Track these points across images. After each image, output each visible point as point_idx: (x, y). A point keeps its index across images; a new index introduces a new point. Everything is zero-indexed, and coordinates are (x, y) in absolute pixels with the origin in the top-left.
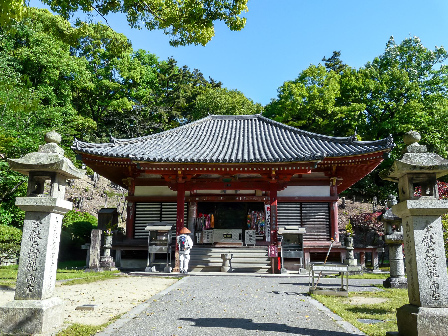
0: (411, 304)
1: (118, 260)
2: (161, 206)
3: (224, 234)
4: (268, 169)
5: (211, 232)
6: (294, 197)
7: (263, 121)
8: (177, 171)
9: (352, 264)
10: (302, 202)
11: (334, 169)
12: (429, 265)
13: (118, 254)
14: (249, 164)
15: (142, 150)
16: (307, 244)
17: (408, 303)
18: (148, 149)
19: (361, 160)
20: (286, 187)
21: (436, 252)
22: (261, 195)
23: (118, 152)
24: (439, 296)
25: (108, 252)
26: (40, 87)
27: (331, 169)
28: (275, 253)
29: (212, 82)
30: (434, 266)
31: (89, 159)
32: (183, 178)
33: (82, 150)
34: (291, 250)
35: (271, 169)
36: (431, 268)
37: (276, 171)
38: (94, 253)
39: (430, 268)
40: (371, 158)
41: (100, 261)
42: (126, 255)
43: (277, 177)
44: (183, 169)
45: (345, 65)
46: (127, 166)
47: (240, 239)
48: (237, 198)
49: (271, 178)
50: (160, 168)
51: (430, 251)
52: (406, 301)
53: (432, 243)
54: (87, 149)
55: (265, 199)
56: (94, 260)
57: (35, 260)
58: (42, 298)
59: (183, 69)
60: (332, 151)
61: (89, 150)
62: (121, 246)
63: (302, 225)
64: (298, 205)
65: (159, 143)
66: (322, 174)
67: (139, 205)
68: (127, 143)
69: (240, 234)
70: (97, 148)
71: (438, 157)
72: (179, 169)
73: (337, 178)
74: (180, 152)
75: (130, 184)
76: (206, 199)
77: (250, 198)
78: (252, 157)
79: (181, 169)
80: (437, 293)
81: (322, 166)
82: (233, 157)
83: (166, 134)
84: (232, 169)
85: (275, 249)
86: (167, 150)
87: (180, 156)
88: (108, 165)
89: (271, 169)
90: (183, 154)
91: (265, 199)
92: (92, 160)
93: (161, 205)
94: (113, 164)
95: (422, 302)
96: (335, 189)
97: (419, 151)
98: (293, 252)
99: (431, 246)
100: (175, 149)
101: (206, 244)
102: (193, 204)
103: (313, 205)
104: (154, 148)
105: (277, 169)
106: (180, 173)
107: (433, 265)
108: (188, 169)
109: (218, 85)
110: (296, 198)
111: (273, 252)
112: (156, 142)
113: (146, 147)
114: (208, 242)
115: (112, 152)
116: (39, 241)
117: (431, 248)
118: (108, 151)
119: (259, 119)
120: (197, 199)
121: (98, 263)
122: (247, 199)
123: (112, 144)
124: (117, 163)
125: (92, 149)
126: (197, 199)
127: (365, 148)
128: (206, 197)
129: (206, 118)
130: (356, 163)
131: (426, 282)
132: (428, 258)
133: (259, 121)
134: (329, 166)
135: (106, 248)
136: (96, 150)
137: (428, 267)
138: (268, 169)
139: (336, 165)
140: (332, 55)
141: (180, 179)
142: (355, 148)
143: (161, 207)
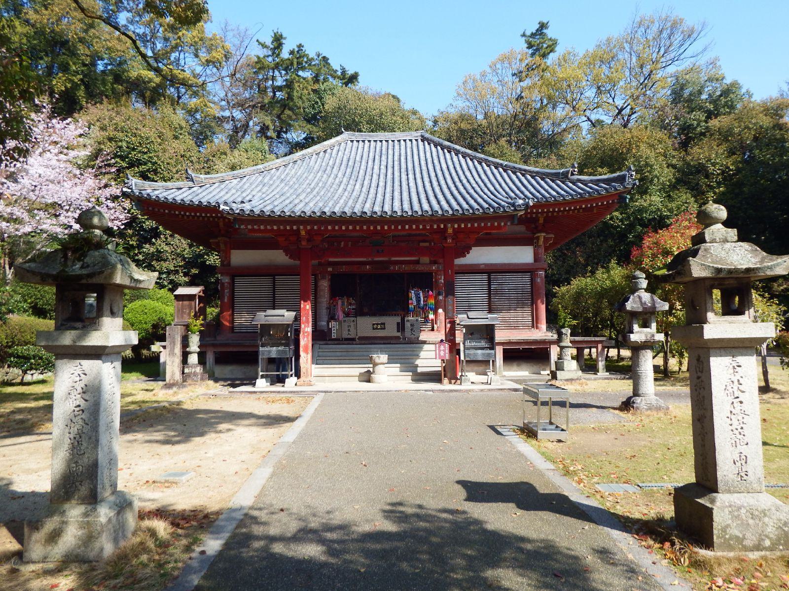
0: (698, 484)
1: (210, 367)
3: (374, 324)
4: (442, 226)
5: (353, 321)
7: (430, 142)
8: (298, 229)
9: (569, 369)
10: (491, 271)
11: (541, 221)
12: (733, 427)
13: (210, 358)
14: (423, 232)
15: (239, 193)
16: (501, 336)
17: (692, 479)
18: (249, 191)
19: (584, 206)
20: (468, 253)
21: (744, 407)
23: (201, 196)
24: (746, 475)
25: (193, 359)
27: (536, 220)
29: (344, 72)
30: (742, 428)
31: (153, 209)
32: (309, 240)
36: (736, 432)
37: (454, 229)
38: (173, 362)
39: (736, 432)
40: (600, 204)
41: (183, 373)
42: (223, 359)
43: (454, 237)
46: (216, 219)
47: (398, 331)
49: (446, 239)
50: (272, 226)
51: (735, 405)
52: (687, 475)
53: (739, 392)
54: (148, 191)
56: (173, 374)
57: (80, 437)
58: (98, 500)
59: (296, 49)
61: (153, 195)
62: (214, 345)
63: (490, 311)
64: (485, 277)
65: (266, 181)
66: (522, 228)
67: (237, 280)
69: (398, 324)
71: (757, 250)
72: (301, 227)
73: (543, 234)
74: (301, 197)
75: (222, 246)
76: (343, 269)
77: (411, 267)
78: (416, 207)
79: (305, 228)
80: (744, 470)
82: (387, 208)
83: (277, 165)
84: (386, 228)
87: (302, 205)
88: (185, 217)
90: (307, 200)
92: (159, 210)
94: (193, 217)
95: (720, 485)
97: (726, 241)
98: (480, 352)
99: (738, 397)
100: (292, 191)
101: (347, 339)
102: (323, 278)
104: (259, 188)
105: (456, 226)
106: (303, 233)
107: (739, 427)
108: (315, 227)
109: (353, 78)
110: (482, 267)
112: (261, 178)
113: (246, 187)
114: (349, 337)
115: (190, 198)
117: (738, 400)
118: (185, 195)
119: (424, 139)
120: (330, 269)
121: (178, 376)
122: (406, 268)
123: (191, 184)
124: (201, 214)
125: (156, 192)
126: (330, 269)
127: (591, 188)
129: (339, 138)
130: (576, 211)
131: (728, 455)
132: (733, 417)
133: (423, 141)
134: (534, 216)
135: (190, 353)
136: (165, 194)
137: (732, 431)
138: (442, 226)
139: (545, 215)
140: (537, 26)
141: (304, 243)
142: (574, 187)
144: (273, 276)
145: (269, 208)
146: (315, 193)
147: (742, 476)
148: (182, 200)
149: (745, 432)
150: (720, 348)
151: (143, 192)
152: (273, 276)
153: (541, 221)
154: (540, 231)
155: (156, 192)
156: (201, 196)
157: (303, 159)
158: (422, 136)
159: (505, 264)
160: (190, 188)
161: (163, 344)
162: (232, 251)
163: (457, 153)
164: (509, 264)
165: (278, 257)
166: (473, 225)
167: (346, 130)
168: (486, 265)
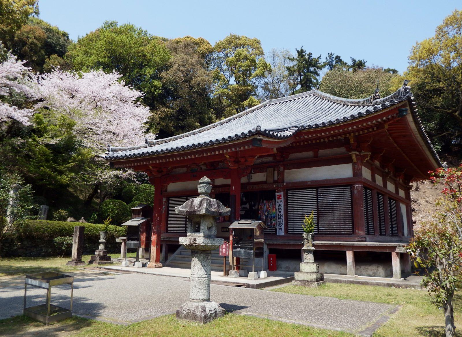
3: (222, 231)
6: (307, 182)
14: (393, 108)
22: (272, 181)
26: (83, 53)
28: (226, 252)
34: (242, 248)
45: (125, 86)
48: (248, 187)
55: (275, 186)
60: (294, 130)
81: (326, 140)
85: (226, 246)
91: (275, 186)
103: (332, 190)
111: (224, 250)
128: (220, 189)
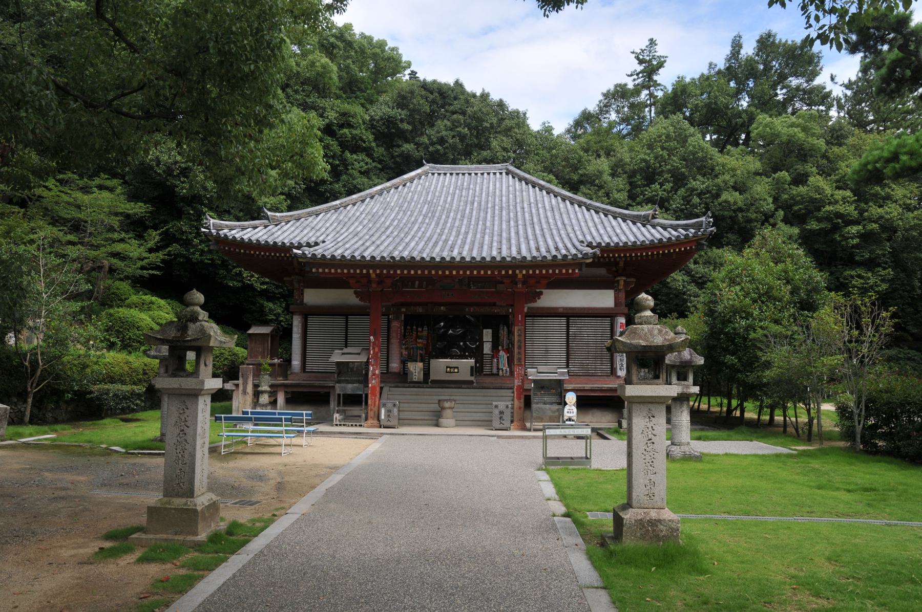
2: (347, 321)
6: (558, 308)
10: (569, 314)
11: (622, 264)
15: (314, 231)
18: (324, 229)
23: (276, 235)
27: (617, 263)
33: (218, 233)
35: (514, 272)
44: (378, 271)
47: (472, 375)
49: (516, 284)
54: (226, 231)
64: (564, 320)
66: (602, 271)
67: (311, 319)
68: (289, 219)
70: (243, 229)
72: (371, 271)
73: (624, 278)
86: (354, 233)
89: (514, 272)
93: (347, 318)
96: (622, 295)
103: (587, 321)
105: (524, 272)
106: (373, 276)
108: (385, 272)
115: (265, 237)
116: (187, 430)
118: (260, 234)
126: (403, 310)
141: (374, 285)
143: (347, 323)
144: (346, 315)
145: (339, 252)
146: (388, 233)
147: (651, 496)
148: (257, 240)
149: (655, 464)
150: (639, 403)
151: (221, 232)
152: (346, 315)
153: (622, 264)
154: (621, 275)
155: (233, 232)
156: (276, 235)
157: (380, 193)
158: (507, 169)
159: (584, 308)
160: (266, 227)
161: (236, 382)
162: (306, 290)
163: (541, 188)
164: (589, 309)
165: (347, 297)
166: (534, 272)
167: (428, 162)
168: (564, 308)
